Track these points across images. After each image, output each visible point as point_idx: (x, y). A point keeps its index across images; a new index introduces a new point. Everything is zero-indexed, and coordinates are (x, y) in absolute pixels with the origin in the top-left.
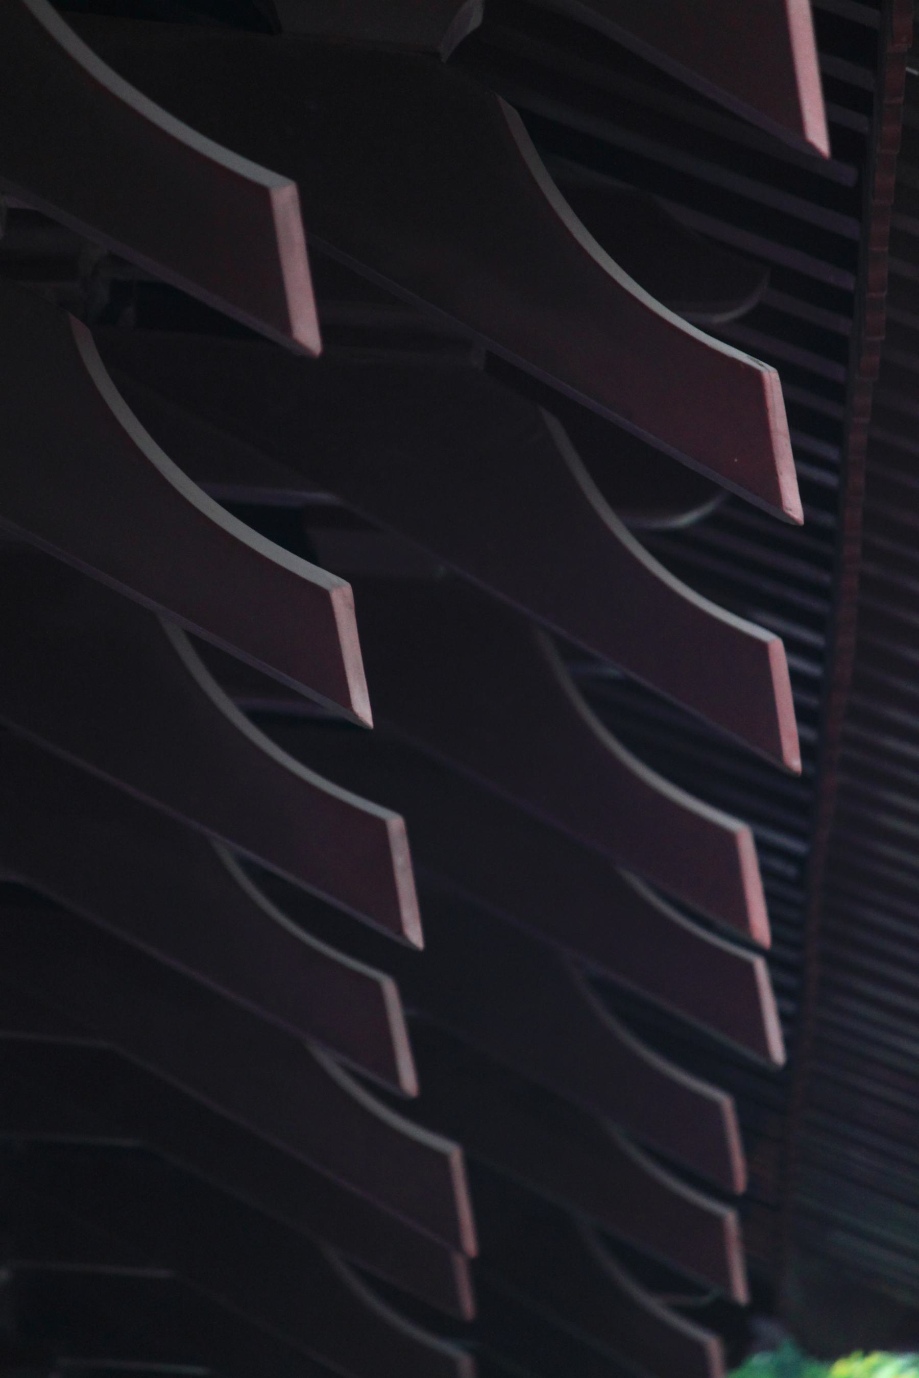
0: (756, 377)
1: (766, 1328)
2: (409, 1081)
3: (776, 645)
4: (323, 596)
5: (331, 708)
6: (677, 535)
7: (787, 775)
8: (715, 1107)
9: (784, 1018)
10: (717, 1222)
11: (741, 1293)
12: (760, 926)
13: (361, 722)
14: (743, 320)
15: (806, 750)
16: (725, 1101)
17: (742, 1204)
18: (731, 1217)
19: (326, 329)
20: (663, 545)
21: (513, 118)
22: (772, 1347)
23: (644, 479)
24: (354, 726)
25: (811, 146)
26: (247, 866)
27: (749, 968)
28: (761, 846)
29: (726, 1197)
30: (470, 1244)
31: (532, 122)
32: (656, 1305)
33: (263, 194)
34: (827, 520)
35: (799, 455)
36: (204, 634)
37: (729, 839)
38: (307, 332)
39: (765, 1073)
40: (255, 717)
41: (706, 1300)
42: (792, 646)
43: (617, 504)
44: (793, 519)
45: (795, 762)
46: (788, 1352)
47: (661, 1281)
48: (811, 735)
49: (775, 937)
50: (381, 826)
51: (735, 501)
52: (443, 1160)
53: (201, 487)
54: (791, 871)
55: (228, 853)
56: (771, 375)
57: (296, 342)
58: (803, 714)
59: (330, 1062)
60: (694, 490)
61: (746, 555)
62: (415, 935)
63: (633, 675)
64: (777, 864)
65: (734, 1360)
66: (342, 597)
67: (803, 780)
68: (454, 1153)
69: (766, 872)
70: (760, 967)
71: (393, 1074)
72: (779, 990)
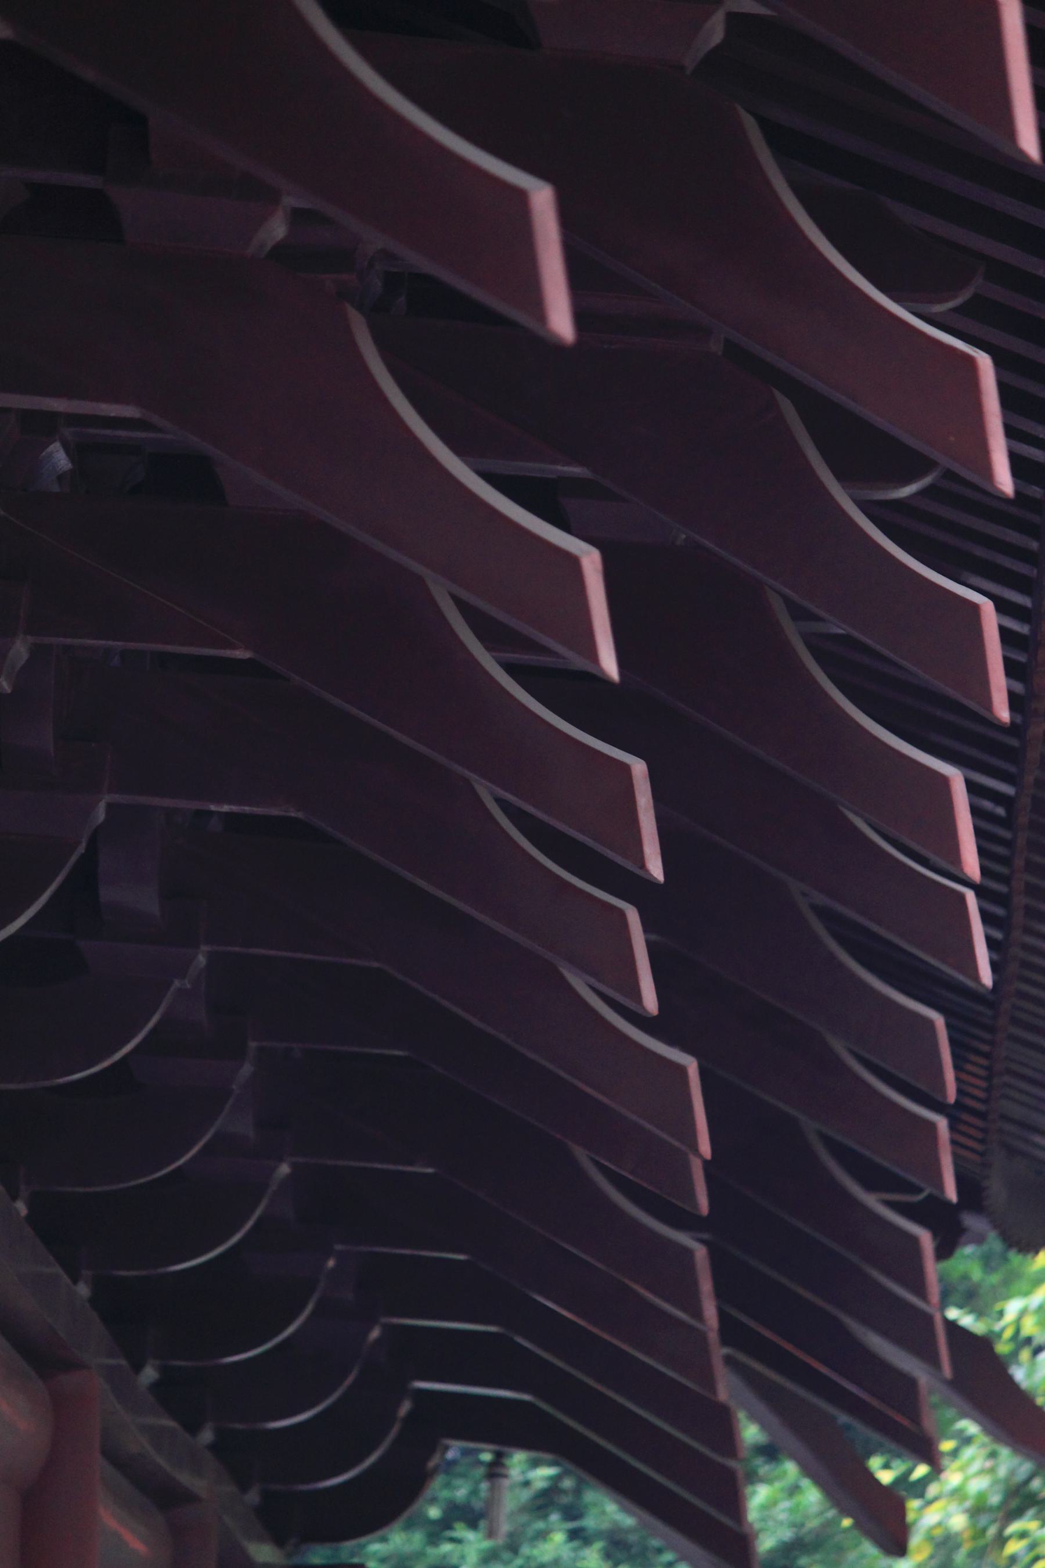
0: (970, 363)
1: (971, 1221)
2: (650, 1001)
3: (987, 606)
4: (573, 563)
5: (578, 662)
6: (898, 505)
7: (996, 725)
8: (930, 1024)
9: (992, 944)
10: (932, 1126)
11: (951, 1194)
12: (971, 863)
13: (607, 676)
14: (955, 310)
15: (1015, 701)
16: (938, 1020)
17: (953, 1113)
18: (942, 1123)
19: (580, 317)
20: (883, 515)
21: (750, 124)
22: (980, 1240)
23: (870, 455)
24: (600, 680)
25: (1022, 153)
26: (500, 802)
27: (962, 898)
28: (972, 787)
29: (939, 1107)
30: (705, 1147)
31: (764, 124)
32: (872, 1201)
33: (521, 197)
34: (1035, 491)
35: (1010, 432)
36: (465, 595)
37: (944, 782)
38: (561, 323)
39: (977, 996)
40: (511, 669)
41: (921, 1196)
42: (1002, 606)
43: (841, 476)
44: (1003, 493)
45: (1003, 713)
46: (994, 1243)
47: (875, 1179)
48: (1019, 687)
49: (984, 870)
50: (625, 769)
51: (949, 475)
52: (681, 1071)
53: (462, 460)
54: (1000, 811)
55: (485, 792)
56: (985, 362)
57: (965, 874)
58: (1011, 669)
59: (579, 983)
60: (913, 465)
61: (957, 525)
62: (656, 869)
63: (856, 634)
64: (987, 805)
65: (944, 1251)
66: (591, 562)
67: (1013, 729)
68: (692, 1065)
69: (976, 812)
70: (970, 897)
71: (636, 993)
72: (987, 918)
